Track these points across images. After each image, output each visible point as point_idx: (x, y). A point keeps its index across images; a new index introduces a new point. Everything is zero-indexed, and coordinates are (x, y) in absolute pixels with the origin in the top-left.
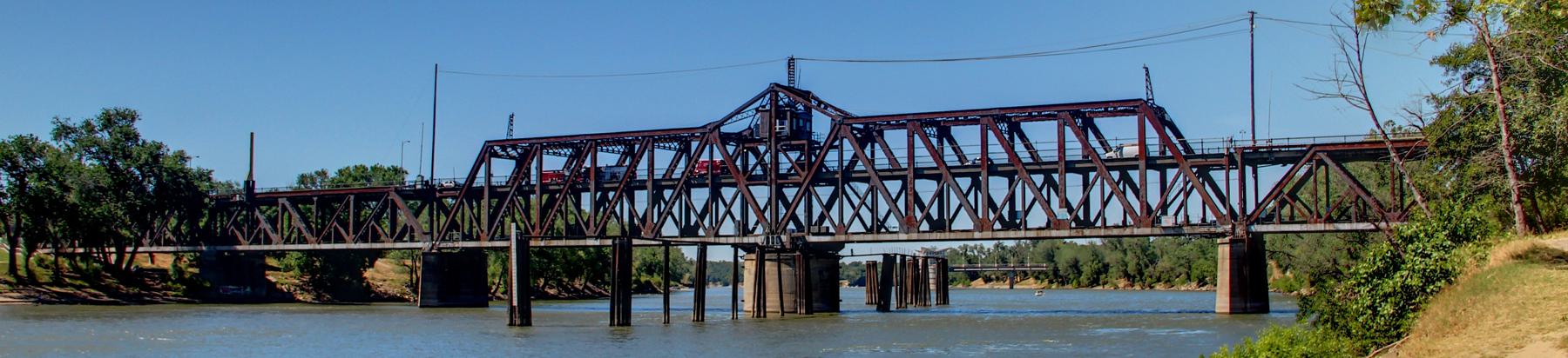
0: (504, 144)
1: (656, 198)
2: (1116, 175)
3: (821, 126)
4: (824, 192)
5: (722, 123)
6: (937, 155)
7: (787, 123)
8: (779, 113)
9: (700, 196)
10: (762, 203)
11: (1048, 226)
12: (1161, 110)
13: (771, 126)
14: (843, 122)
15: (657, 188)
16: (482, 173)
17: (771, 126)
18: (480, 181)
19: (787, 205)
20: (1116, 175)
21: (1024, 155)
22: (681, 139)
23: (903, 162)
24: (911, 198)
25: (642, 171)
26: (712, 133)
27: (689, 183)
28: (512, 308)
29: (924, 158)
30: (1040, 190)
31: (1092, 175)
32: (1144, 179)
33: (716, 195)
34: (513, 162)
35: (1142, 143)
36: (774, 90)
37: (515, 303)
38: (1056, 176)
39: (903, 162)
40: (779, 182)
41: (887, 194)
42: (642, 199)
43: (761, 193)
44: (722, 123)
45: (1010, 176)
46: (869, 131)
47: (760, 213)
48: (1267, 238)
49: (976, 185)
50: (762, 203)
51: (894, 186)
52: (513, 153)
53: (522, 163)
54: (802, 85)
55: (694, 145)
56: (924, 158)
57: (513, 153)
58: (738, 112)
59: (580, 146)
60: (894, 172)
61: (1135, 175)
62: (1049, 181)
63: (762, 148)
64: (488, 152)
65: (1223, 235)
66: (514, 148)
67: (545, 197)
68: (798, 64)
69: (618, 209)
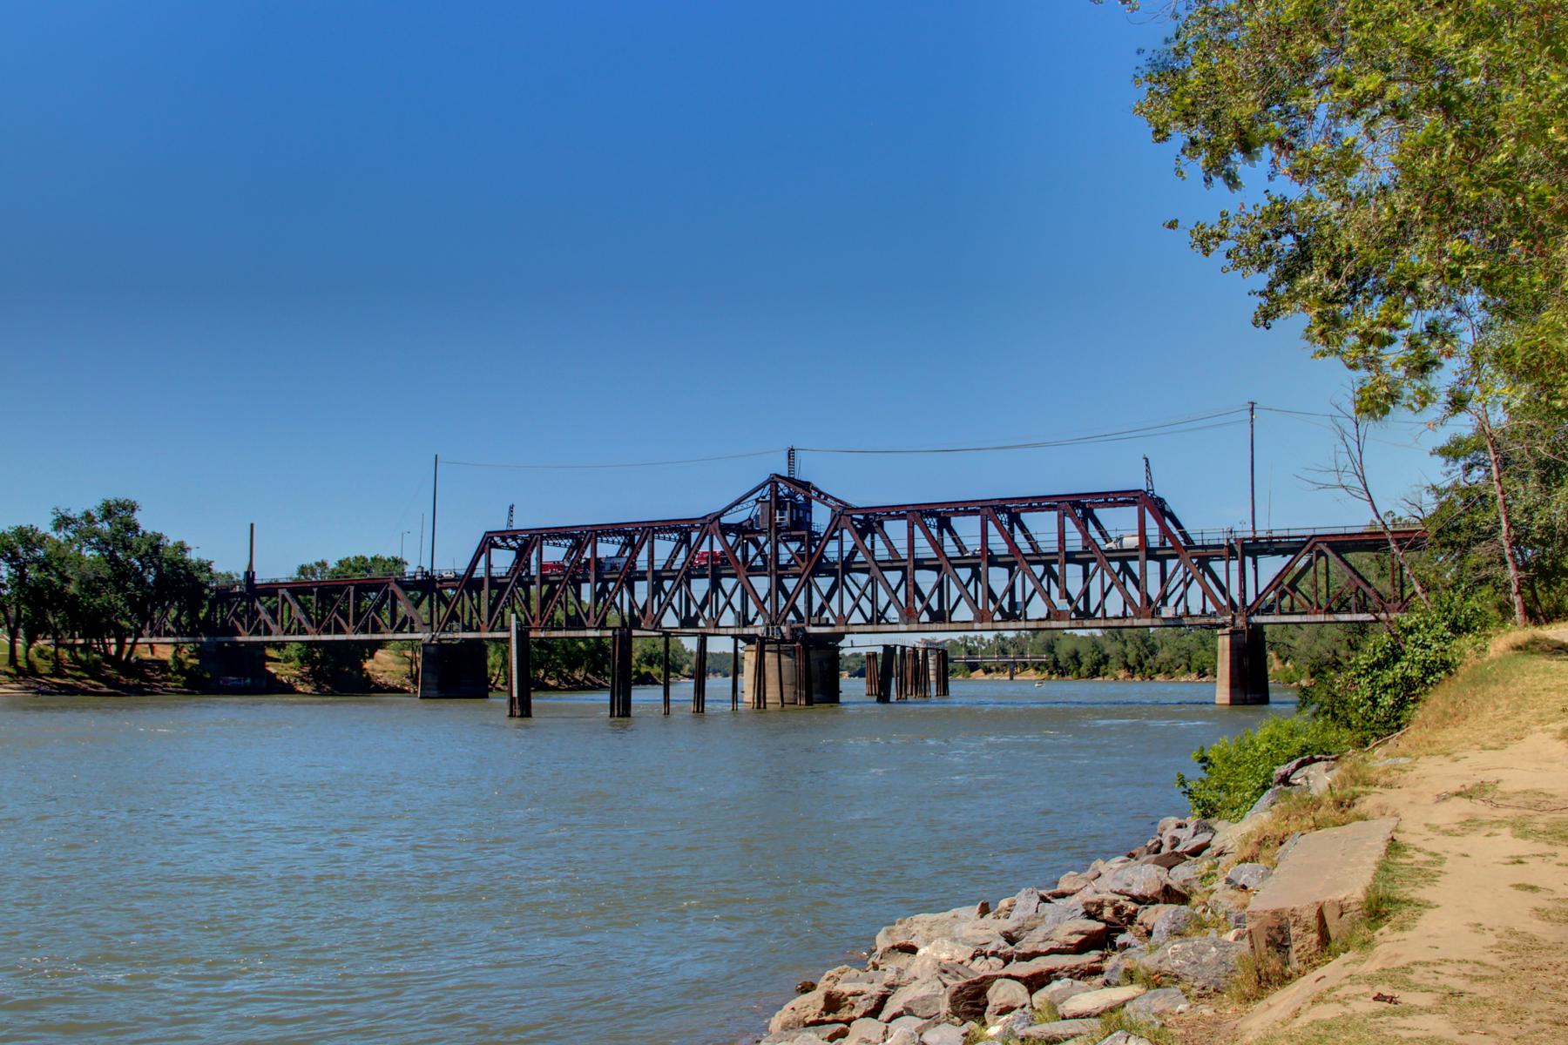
0: (504, 535)
1: (656, 589)
2: (1039, 570)
3: (821, 517)
4: (824, 583)
5: (722, 514)
6: (937, 546)
7: (787, 513)
8: (779, 504)
9: (700, 587)
10: (762, 594)
11: (1048, 617)
12: (1161, 500)
13: (771, 517)
14: (843, 513)
15: (658, 579)
16: (482, 564)
17: (771, 517)
18: (480, 571)
19: (787, 596)
20: (1116, 566)
21: (1024, 546)
22: (681, 530)
23: (903, 553)
24: (911, 589)
25: (642, 562)
26: (712, 524)
27: (689, 574)
28: (512, 700)
29: (924, 549)
30: (1040, 580)
31: (1092, 566)
32: (1143, 569)
33: (716, 586)
34: (513, 553)
35: (1062, 538)
36: (774, 480)
37: (515, 694)
38: (1056, 567)
39: (903, 553)
40: (779, 573)
41: (887, 585)
42: (642, 589)
43: (762, 584)
44: (722, 514)
45: (1010, 567)
46: (869, 522)
47: (760, 604)
48: (1267, 629)
49: (976, 575)
50: (762, 594)
51: (894, 577)
52: (513, 544)
53: (522, 553)
54: (802, 476)
55: (694, 535)
56: (924, 549)
57: (513, 544)
58: (738, 502)
59: (581, 537)
60: (894, 564)
61: (1135, 566)
62: (1049, 572)
63: (762, 539)
64: (488, 543)
65: (1223, 626)
66: (514, 538)
67: (545, 588)
68: (798, 454)
69: (618, 600)
